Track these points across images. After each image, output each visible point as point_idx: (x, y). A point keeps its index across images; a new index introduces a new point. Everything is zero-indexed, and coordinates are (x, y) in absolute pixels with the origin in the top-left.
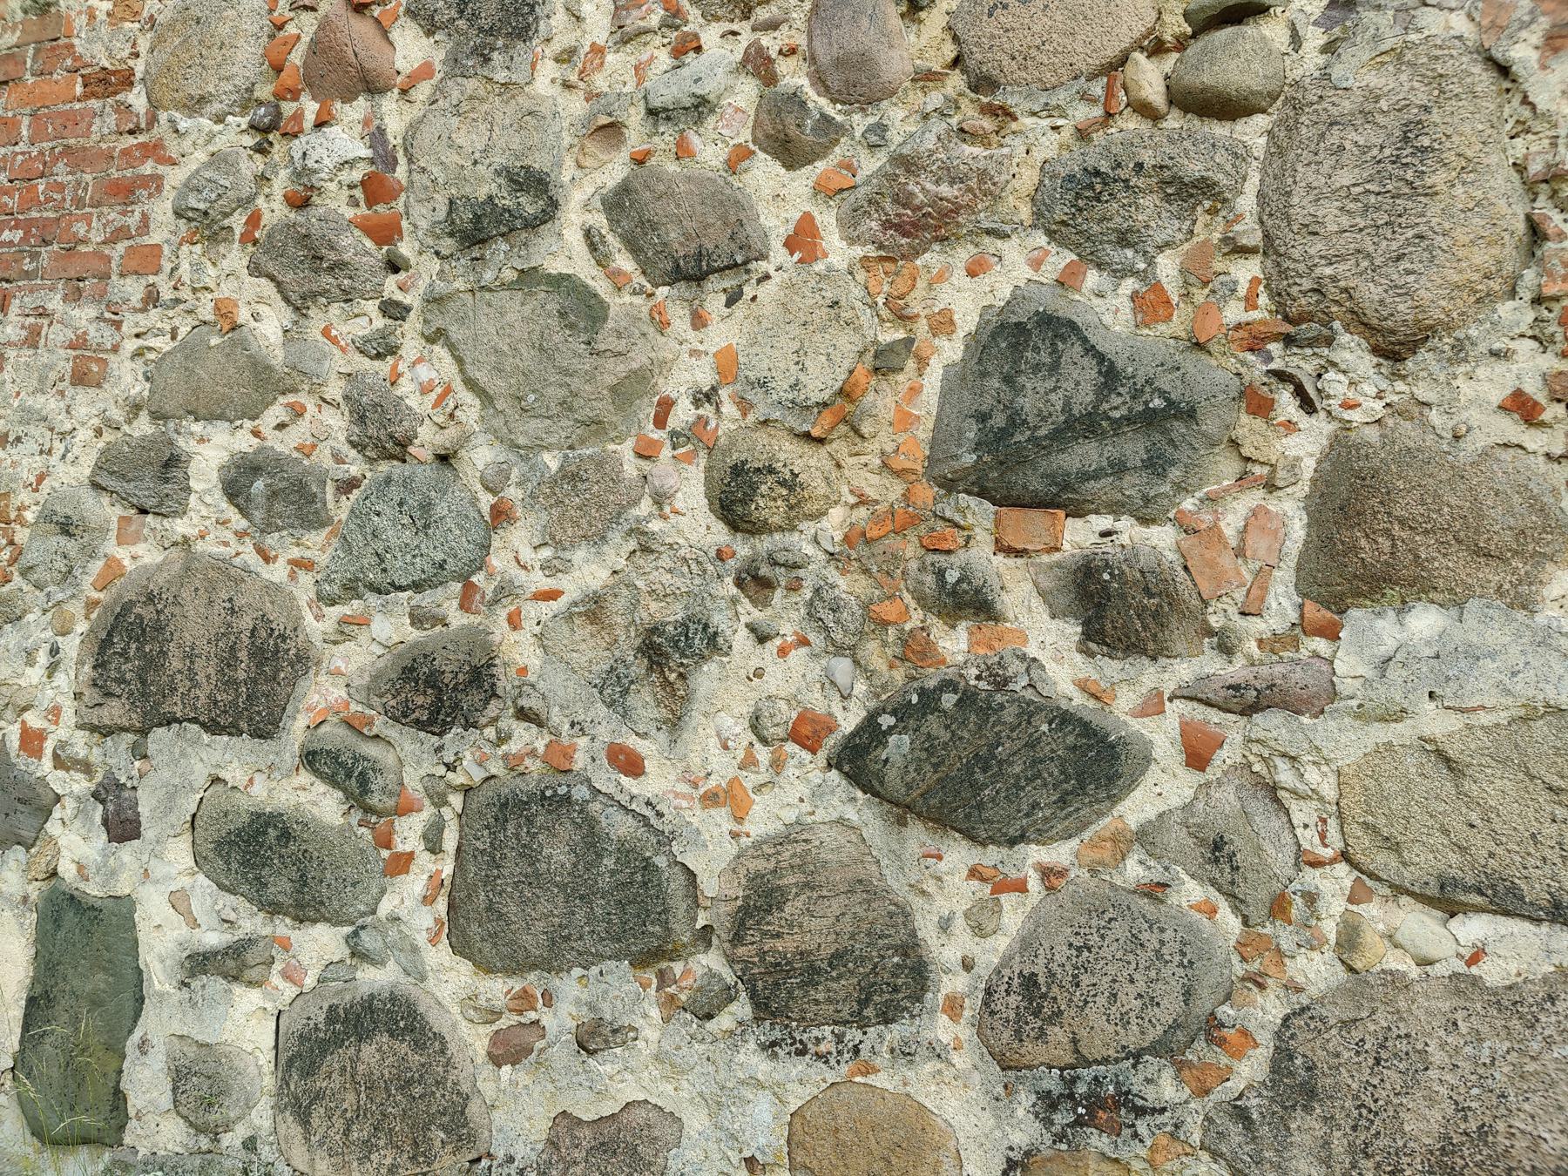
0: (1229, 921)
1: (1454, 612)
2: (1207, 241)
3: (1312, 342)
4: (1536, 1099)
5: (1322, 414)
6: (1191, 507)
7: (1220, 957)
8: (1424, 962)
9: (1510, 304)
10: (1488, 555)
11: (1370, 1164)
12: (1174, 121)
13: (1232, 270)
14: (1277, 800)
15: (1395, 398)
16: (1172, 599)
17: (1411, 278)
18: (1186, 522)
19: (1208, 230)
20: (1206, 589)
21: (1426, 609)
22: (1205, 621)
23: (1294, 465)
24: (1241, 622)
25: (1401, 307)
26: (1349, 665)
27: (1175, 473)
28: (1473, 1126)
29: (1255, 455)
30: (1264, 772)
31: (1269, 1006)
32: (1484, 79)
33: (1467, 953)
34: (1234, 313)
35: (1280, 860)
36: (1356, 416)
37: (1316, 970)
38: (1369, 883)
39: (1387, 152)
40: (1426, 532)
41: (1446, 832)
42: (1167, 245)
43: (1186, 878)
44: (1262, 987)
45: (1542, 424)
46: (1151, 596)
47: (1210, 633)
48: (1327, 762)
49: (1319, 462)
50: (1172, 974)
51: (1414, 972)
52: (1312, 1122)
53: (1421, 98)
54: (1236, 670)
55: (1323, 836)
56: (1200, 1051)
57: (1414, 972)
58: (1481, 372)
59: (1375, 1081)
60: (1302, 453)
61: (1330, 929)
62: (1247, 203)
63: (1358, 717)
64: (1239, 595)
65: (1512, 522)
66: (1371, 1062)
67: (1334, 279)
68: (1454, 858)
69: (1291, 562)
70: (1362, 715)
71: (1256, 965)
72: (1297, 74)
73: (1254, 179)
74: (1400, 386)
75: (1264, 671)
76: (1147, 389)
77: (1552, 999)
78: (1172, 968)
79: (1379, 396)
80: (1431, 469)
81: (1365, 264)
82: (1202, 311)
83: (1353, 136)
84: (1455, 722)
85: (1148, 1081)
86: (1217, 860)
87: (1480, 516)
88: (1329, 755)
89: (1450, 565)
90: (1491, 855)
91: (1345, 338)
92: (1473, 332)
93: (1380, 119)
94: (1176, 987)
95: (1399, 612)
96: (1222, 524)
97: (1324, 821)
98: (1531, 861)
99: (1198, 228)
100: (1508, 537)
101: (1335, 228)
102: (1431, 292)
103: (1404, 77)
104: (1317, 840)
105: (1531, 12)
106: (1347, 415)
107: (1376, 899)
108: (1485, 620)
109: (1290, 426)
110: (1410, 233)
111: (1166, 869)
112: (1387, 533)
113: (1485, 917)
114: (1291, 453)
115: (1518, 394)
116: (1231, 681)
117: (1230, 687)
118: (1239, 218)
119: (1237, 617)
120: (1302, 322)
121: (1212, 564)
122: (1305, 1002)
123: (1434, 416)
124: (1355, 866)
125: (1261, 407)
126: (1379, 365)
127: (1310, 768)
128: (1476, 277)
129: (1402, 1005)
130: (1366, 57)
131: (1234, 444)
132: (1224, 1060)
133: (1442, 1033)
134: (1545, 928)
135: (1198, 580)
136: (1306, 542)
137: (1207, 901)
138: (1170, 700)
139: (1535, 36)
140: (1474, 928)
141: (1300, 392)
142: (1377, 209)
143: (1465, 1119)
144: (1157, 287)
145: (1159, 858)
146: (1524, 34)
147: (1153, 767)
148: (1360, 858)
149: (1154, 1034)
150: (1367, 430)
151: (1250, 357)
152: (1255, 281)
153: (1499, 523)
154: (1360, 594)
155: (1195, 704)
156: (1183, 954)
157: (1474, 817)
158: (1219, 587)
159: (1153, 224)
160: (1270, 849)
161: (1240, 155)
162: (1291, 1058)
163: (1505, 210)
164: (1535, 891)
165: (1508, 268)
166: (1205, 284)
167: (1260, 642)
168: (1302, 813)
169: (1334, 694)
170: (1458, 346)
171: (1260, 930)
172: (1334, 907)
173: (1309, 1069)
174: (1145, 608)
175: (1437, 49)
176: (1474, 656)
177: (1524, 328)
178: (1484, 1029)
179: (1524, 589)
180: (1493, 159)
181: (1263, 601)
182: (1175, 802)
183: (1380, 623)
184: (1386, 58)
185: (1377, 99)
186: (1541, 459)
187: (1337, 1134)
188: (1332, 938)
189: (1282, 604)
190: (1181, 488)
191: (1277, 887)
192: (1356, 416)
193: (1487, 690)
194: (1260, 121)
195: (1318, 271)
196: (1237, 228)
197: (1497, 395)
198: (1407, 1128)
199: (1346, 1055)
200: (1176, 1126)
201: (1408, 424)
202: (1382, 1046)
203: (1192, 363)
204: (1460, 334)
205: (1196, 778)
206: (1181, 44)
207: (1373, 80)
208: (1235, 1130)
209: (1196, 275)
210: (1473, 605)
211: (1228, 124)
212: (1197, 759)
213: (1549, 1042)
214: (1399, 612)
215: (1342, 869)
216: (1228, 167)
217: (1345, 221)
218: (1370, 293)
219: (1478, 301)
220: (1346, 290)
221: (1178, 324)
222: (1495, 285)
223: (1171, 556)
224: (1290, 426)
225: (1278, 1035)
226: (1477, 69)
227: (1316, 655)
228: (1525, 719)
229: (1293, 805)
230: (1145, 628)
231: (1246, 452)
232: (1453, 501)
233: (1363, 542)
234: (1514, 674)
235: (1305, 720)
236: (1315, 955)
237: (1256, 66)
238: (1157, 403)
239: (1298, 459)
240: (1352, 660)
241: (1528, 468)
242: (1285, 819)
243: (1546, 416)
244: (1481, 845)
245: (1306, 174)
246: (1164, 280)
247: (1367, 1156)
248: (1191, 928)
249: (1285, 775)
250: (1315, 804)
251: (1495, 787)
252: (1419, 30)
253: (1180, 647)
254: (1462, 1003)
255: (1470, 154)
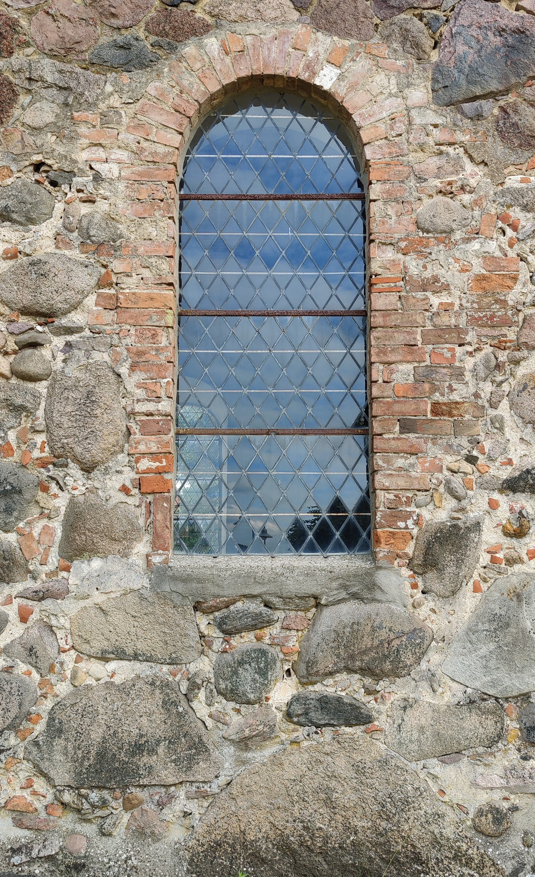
0: (36, 676)
1: (105, 560)
2: (26, 427)
3: (61, 466)
4: (130, 719)
5: (66, 491)
6: (22, 526)
7: (33, 689)
8: (98, 680)
9: (122, 455)
10: (115, 540)
11: (80, 752)
12: (14, 381)
13: (35, 438)
14: (52, 631)
15: (89, 486)
16: (14, 561)
17: (90, 446)
18: (20, 531)
19: (26, 423)
20: (27, 556)
21: (97, 559)
22: (27, 568)
23: (57, 509)
24: (40, 567)
25: (87, 456)
26: (73, 580)
27: (15, 514)
28: (112, 731)
29: (44, 506)
30: (48, 621)
31: (48, 704)
32: (112, 377)
33: (110, 674)
34: (36, 454)
35: (52, 651)
36: (76, 492)
37: (63, 689)
38: (81, 655)
39: (82, 401)
40: (96, 533)
41: (103, 635)
42: (11, 427)
43: (20, 663)
44: (46, 698)
45: (132, 495)
46: (6, 560)
47: (30, 572)
48: (67, 615)
49: (66, 508)
50: (15, 700)
51: (94, 683)
52: (62, 742)
53: (93, 383)
54: (36, 585)
55: (66, 641)
56: (26, 725)
57: (94, 683)
58: (114, 478)
59: (82, 723)
60: (60, 505)
61: (68, 673)
62: (40, 413)
63: (75, 599)
64: (39, 558)
65: (122, 529)
66: (80, 716)
67: (67, 444)
68: (106, 643)
69: (57, 545)
70: (76, 598)
71: (44, 690)
72: (54, 368)
73: (43, 404)
74: (90, 482)
75: (46, 585)
76: (5, 482)
77: (134, 685)
78: (15, 696)
79: (84, 485)
80: (98, 511)
81: (77, 439)
82: (24, 453)
83: (72, 394)
84: (104, 597)
85: (5, 740)
86: (31, 655)
87: (112, 527)
88: (65, 613)
89: (104, 544)
90: (117, 640)
91: (71, 465)
92: (110, 465)
93: (80, 389)
94: (16, 703)
95: (89, 561)
96: (33, 532)
97: (67, 636)
98: (128, 641)
99: (22, 422)
100: (121, 534)
101: (67, 426)
102: (96, 451)
103: (87, 375)
104: (64, 643)
105: (127, 356)
106: (74, 492)
107: (84, 661)
108: (113, 562)
109: (55, 496)
110: (89, 430)
111: (13, 661)
112: (84, 534)
113: (116, 661)
114: (57, 505)
115: (124, 486)
116: (35, 590)
117: (34, 592)
118: (37, 419)
119: (39, 566)
120: (59, 458)
121: (29, 547)
122: (59, 700)
123: (100, 493)
124: (77, 650)
125: (45, 489)
126: (83, 474)
127: (61, 618)
128: (110, 446)
129: (90, 695)
130: (75, 367)
131: (37, 502)
132: (31, 726)
133: (102, 702)
134: (132, 662)
135: (25, 553)
136: (62, 537)
137: (28, 671)
138: (15, 598)
139: (127, 365)
140: (112, 666)
141: (58, 483)
142: (80, 421)
143: (110, 730)
144: (8, 443)
145: (11, 657)
146: (124, 364)
147: (9, 623)
148: (77, 647)
149: (8, 722)
150: (80, 497)
151: (42, 470)
152: (44, 442)
153: (118, 530)
154: (76, 556)
155: (23, 599)
156: (19, 691)
157: (111, 629)
158: (32, 555)
159: (5, 420)
160: (49, 648)
161: (36, 396)
162: (54, 720)
163: (119, 423)
164: (130, 651)
165: (121, 443)
166: (25, 443)
167: (46, 574)
168: (60, 634)
169: (68, 592)
170: (106, 469)
171: (46, 678)
172: (70, 665)
173: (60, 723)
174: (4, 565)
175: (98, 365)
176: (110, 574)
177: (126, 463)
178: (115, 699)
179: (126, 551)
180: (116, 406)
181: (46, 559)
182: (17, 636)
183: (83, 565)
184: (82, 367)
185: (79, 382)
186: (133, 507)
187: (69, 744)
188: (69, 676)
189: (54, 560)
190: (18, 519)
191: (51, 661)
192: (76, 492)
193: (114, 587)
194: (44, 383)
195: (62, 440)
196: (36, 423)
197: (118, 486)
198: (92, 737)
199: (72, 716)
200: (14, 753)
201: (93, 495)
202: (84, 711)
203: (21, 472)
204: (106, 465)
205: (25, 626)
206: (15, 352)
207: (78, 374)
208: (34, 750)
209: (22, 439)
210: (110, 557)
211: (34, 383)
212: (24, 619)
213: (133, 699)
214: (89, 561)
215: (72, 652)
216: (31, 401)
217: (70, 424)
218: (78, 450)
219: (111, 454)
220: (71, 448)
221: (16, 457)
222: (117, 449)
223: (15, 544)
224: (55, 496)
225: (50, 713)
226: (110, 374)
227: (63, 578)
228: (125, 594)
229: (57, 632)
230: (4, 572)
231: (42, 504)
232: (105, 522)
233: (77, 537)
234: (121, 580)
235: (59, 601)
236: (63, 683)
237: (39, 365)
238: (8, 487)
239: (59, 507)
240: (74, 579)
241: (129, 510)
242: (55, 637)
243: (132, 493)
244: (113, 637)
245: (57, 406)
246: (11, 441)
247: (79, 749)
248: (22, 681)
249: (54, 622)
250: (64, 630)
251: (117, 618)
252: (92, 359)
253: (18, 578)
254: (109, 691)
255: (108, 403)
